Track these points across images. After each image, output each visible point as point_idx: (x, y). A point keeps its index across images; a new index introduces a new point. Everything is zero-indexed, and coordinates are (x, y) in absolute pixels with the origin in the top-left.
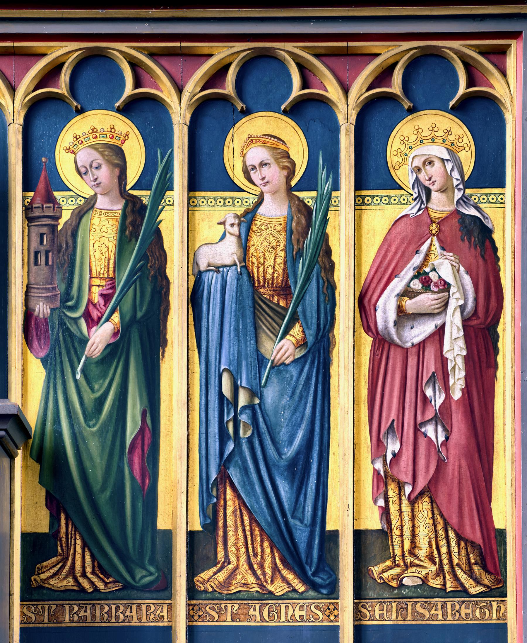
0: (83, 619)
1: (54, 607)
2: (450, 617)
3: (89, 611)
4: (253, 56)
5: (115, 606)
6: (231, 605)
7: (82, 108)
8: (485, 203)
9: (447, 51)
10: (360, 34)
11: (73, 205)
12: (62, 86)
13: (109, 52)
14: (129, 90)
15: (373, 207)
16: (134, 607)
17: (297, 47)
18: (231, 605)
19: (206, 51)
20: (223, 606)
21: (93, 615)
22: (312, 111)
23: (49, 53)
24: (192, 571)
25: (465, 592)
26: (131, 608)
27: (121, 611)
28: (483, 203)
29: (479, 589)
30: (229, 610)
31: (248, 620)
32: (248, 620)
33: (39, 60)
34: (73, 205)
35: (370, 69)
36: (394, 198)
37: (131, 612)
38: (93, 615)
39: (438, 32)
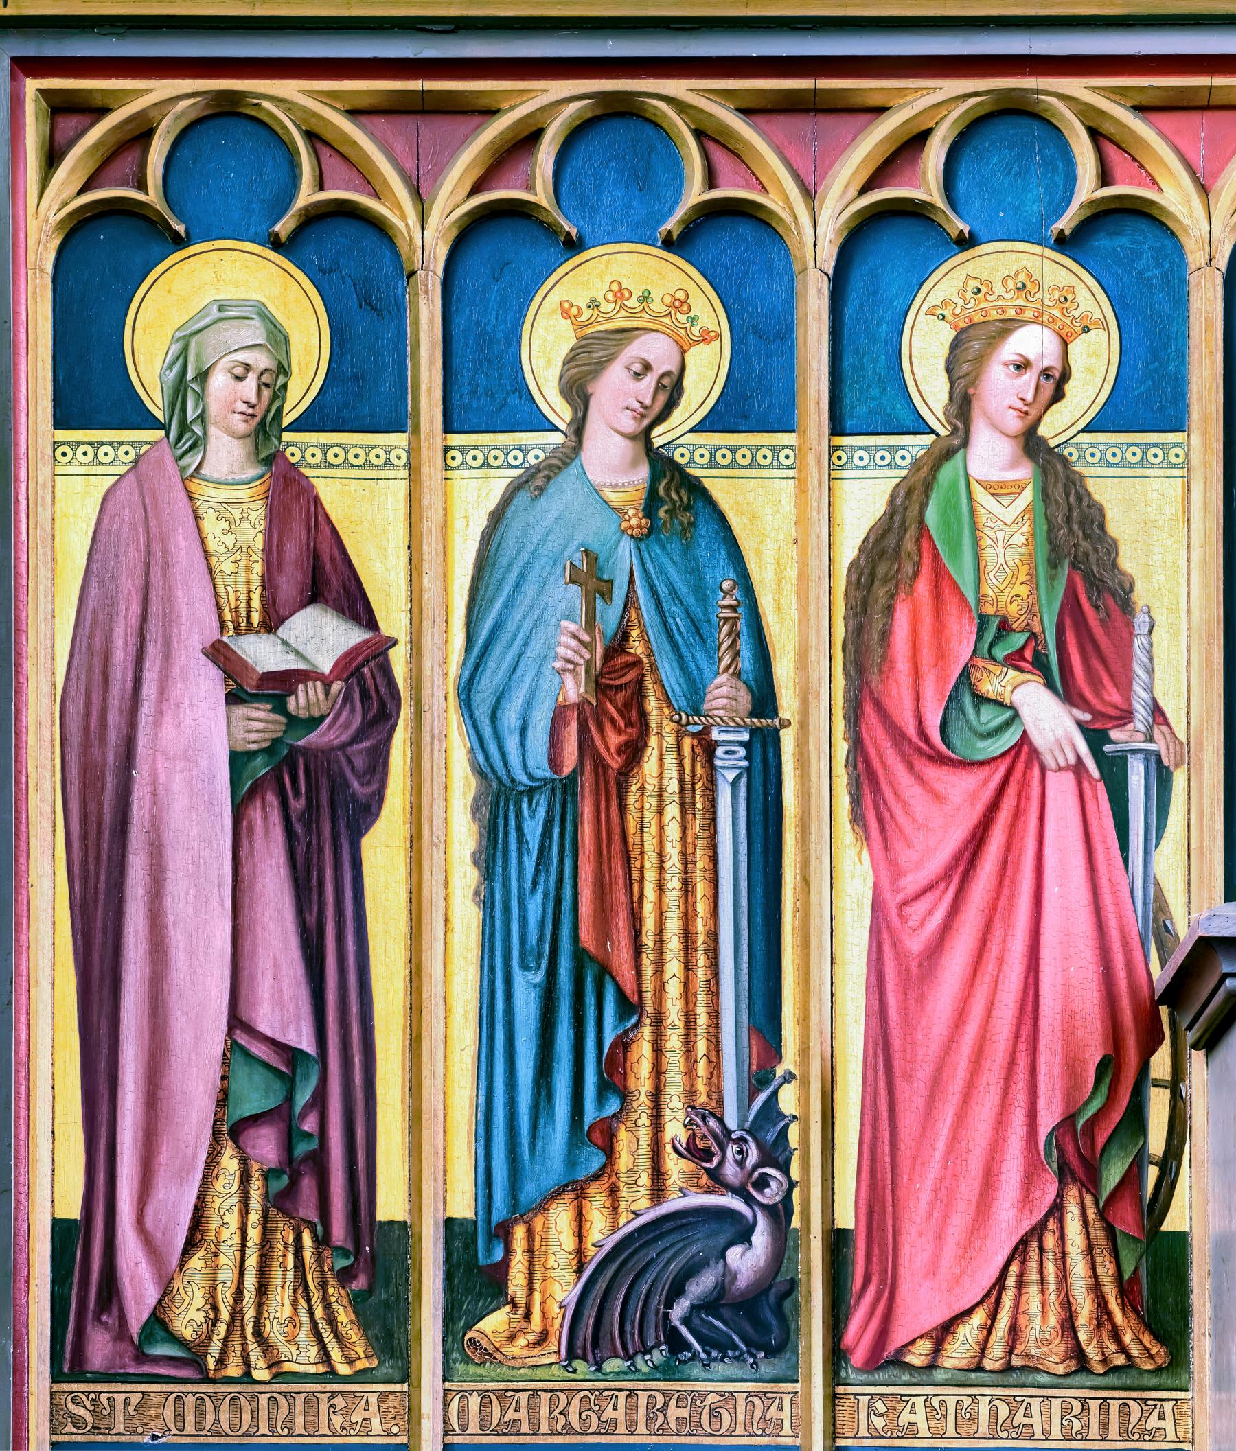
0: (513, 1428)
1: (135, 1399)
2: (642, 1428)
3: (524, 1411)
4: (589, 115)
5: (303, 1396)
6: (124, 1396)
7: (580, 238)
8: (317, 466)
9: (661, 105)
10: (752, 57)
11: (516, 467)
12: (925, 183)
13: (1038, 101)
14: (1087, 188)
15: (466, 473)
16: (787, 1400)
17: (1093, 89)
18: (268, 1396)
19: (875, 101)
20: (104, 1398)
21: (534, 1421)
22: (729, 241)
23: (504, 106)
24: (458, 1317)
25: (332, 1375)
26: (781, 1403)
27: (561, 1408)
28: (1093, 465)
29: (1149, 1366)
30: (119, 1407)
31: (1147, 1438)
32: (1147, 1438)
33: (870, 123)
34: (516, 467)
35: (873, 140)
36: (472, 453)
37: (781, 1409)
38: (534, 1421)
39: (1172, 52)
